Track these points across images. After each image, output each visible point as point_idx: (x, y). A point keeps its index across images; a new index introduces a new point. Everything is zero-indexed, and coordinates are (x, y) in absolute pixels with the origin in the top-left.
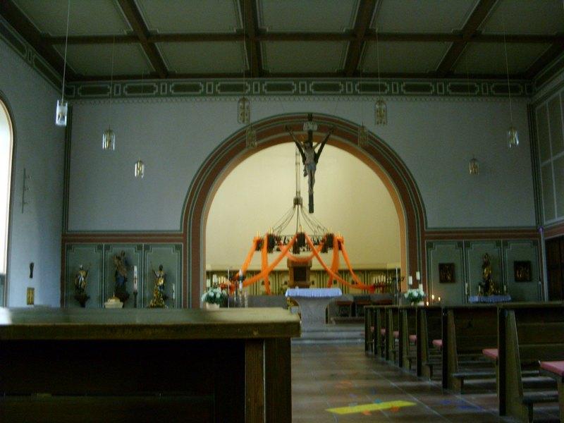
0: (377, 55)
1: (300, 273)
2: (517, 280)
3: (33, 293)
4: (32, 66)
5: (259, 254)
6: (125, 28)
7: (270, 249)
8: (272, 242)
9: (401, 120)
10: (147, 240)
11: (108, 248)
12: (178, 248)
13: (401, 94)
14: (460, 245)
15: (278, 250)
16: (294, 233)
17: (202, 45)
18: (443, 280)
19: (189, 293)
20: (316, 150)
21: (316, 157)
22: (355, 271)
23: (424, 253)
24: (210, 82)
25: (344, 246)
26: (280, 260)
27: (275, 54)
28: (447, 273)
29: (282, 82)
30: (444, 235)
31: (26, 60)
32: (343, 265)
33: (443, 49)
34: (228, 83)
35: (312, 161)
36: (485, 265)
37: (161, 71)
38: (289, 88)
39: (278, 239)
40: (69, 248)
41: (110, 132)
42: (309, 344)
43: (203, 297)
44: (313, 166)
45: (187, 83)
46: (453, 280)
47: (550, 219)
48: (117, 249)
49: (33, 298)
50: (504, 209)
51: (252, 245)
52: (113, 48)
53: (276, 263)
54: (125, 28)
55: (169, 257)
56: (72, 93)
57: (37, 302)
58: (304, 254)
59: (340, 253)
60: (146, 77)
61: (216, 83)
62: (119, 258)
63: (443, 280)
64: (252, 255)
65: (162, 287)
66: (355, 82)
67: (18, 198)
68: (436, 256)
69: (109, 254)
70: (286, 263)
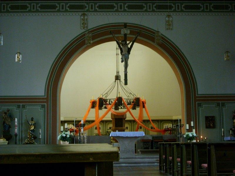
5: (93, 110)
7: (100, 107)
8: (101, 103)
12: (43, 106)
14: (218, 105)
16: (115, 97)
18: (208, 127)
21: (129, 50)
22: (153, 121)
25: (146, 105)
26: (106, 114)
30: (208, 99)
32: (145, 117)
35: (127, 53)
39: (106, 101)
46: (214, 127)
51: (89, 104)
53: (104, 116)
55: (38, 113)
58: (121, 110)
59: (144, 109)
62: (5, 113)
63: (208, 127)
68: (204, 111)
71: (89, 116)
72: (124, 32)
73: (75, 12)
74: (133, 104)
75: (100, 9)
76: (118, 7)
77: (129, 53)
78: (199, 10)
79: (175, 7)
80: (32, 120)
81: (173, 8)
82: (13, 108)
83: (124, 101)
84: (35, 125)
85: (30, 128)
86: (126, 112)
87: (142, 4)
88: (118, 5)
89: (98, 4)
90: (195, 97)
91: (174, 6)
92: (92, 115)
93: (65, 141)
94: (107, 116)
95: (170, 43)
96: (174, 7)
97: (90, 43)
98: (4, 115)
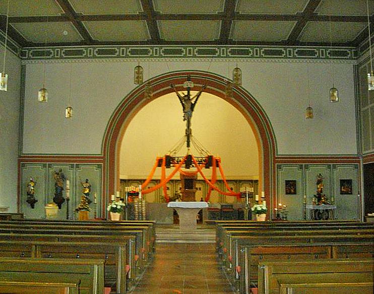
0: (240, 29)
1: (189, 183)
2: (342, 193)
7: (168, 166)
8: (168, 161)
11: (50, 166)
12: (99, 166)
14: (301, 167)
16: (185, 155)
18: (288, 192)
21: (193, 106)
23: (274, 172)
24: (123, 47)
25: (221, 164)
26: (174, 173)
30: (290, 160)
32: (219, 177)
34: (136, 47)
36: (319, 182)
37: (89, 41)
39: (173, 159)
40: (23, 165)
45: (107, 48)
48: (56, 167)
51: (155, 162)
52: (55, 25)
53: (172, 176)
55: (93, 173)
58: (193, 169)
59: (218, 168)
60: (142, 43)
62: (58, 174)
63: (288, 192)
66: (294, 49)
68: (285, 174)
70: (179, 175)
71: (155, 174)
75: (266, 54)
77: (192, 110)
78: (281, 56)
79: (260, 53)
80: (87, 182)
82: (65, 167)
83: (193, 159)
86: (197, 172)
88: (253, 50)
92: (158, 174)
93: (115, 212)
94: (176, 174)
95: (245, 94)
96: (285, 52)
97: (150, 96)
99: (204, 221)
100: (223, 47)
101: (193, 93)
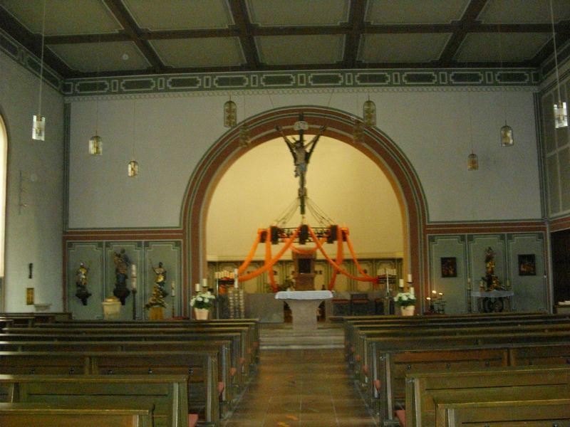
0: (372, 46)
1: (305, 264)
2: (522, 274)
3: (32, 294)
4: (25, 67)
5: (262, 246)
6: (116, 27)
7: (275, 241)
8: (275, 234)
9: (399, 109)
10: (147, 236)
11: (108, 245)
12: (178, 244)
13: (402, 85)
14: (463, 239)
15: (283, 242)
16: (298, 225)
17: (194, 43)
18: (445, 275)
19: (189, 289)
20: (308, 150)
21: (307, 157)
22: (360, 260)
23: (425, 246)
24: (208, 76)
25: (349, 237)
26: (284, 250)
27: (268, 48)
28: (449, 268)
29: (279, 74)
30: (448, 229)
31: (18, 61)
32: (347, 254)
33: (446, 37)
35: (303, 162)
36: (489, 259)
38: (288, 80)
40: (70, 245)
41: (97, 138)
42: (295, 350)
43: (192, 303)
44: (304, 167)
45: (185, 78)
46: (455, 275)
47: (556, 212)
48: (117, 247)
49: (32, 298)
50: (513, 198)
51: (256, 236)
54: (116, 27)
55: (170, 254)
56: (69, 90)
57: (37, 301)
58: (310, 245)
59: (345, 243)
61: (213, 76)
62: (119, 256)
63: (445, 275)
64: (255, 247)
65: (162, 284)
67: (15, 201)
68: (438, 251)
69: (109, 251)
71: (257, 253)
72: (299, 127)
73: (322, 87)
74: (327, 236)
75: (220, 84)
76: (438, 79)
79: (156, 83)
80: (160, 267)
81: (388, 79)
82: (130, 246)
84: (164, 274)
85: (158, 278)
86: (316, 249)
87: (336, 74)
89: (217, 77)
90: (425, 226)
91: (342, 76)
92: (261, 252)
93: (201, 308)
97: (246, 144)
98: (116, 258)
99: (328, 316)
100: (349, 72)
101: (308, 138)
